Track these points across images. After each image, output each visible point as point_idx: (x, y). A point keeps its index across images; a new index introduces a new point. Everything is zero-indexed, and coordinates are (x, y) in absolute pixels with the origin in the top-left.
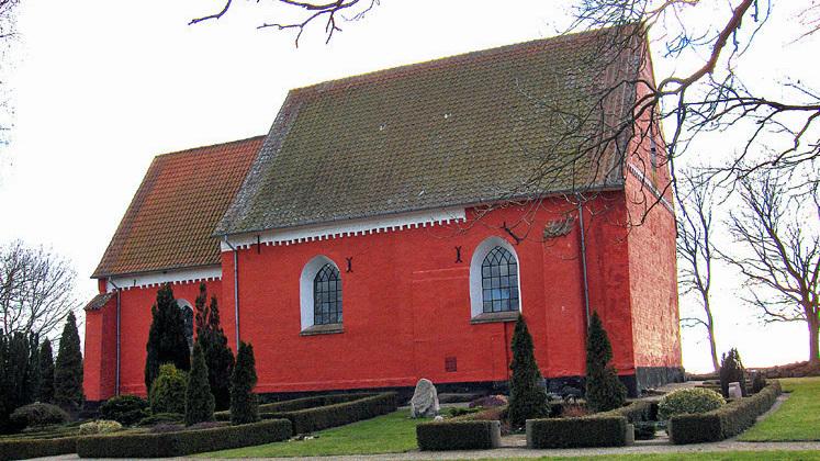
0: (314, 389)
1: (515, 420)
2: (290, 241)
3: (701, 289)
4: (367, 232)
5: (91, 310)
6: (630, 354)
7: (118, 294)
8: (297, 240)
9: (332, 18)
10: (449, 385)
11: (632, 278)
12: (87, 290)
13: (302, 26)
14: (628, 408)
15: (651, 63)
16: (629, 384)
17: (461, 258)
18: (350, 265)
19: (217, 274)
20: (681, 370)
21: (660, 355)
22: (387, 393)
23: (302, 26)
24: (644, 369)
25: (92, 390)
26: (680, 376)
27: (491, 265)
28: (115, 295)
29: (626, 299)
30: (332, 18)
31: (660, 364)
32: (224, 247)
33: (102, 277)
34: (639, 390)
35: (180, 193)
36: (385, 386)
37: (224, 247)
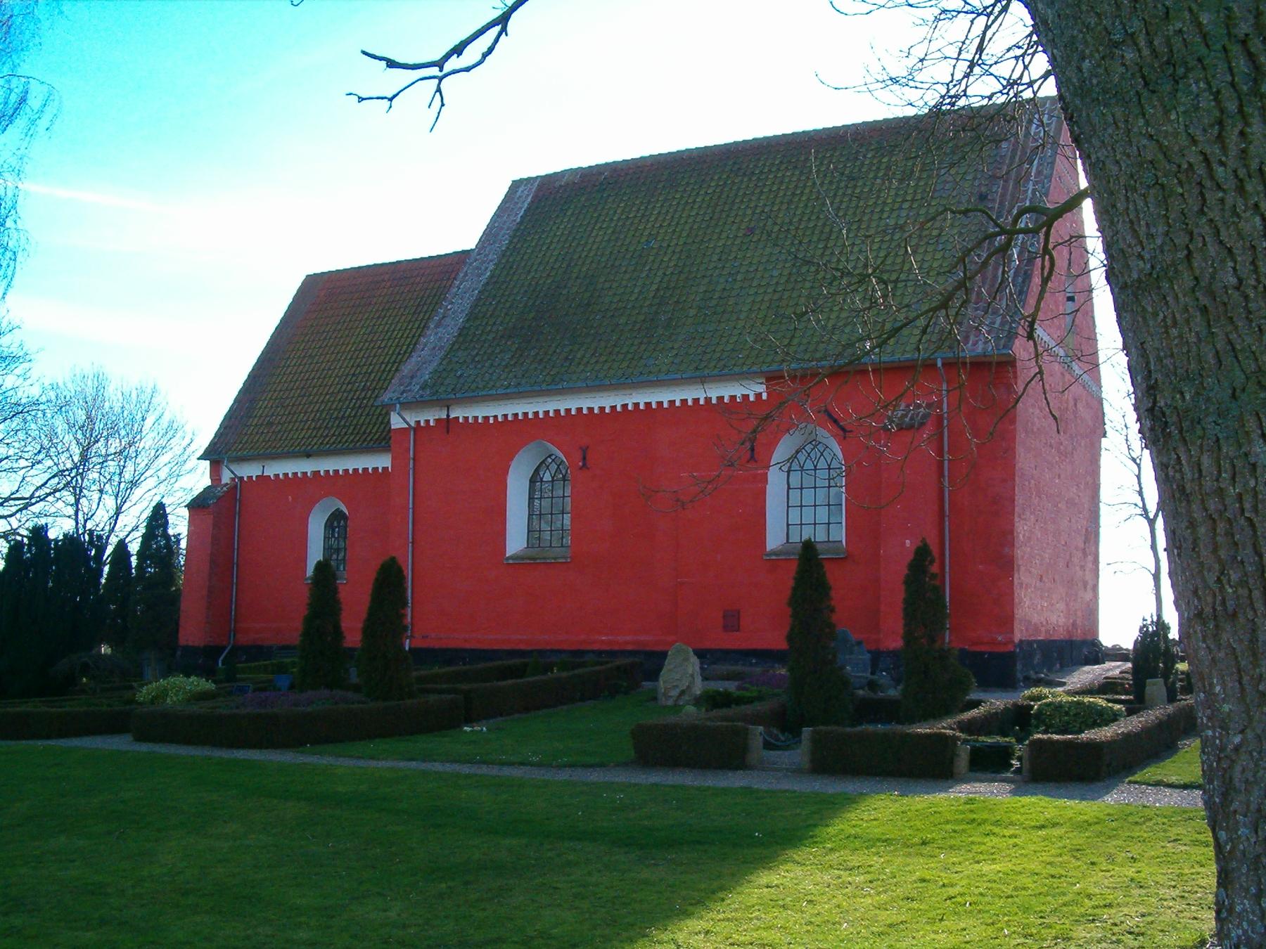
0: (523, 647)
1: (787, 724)
2: (496, 417)
3: (1147, 518)
4: (613, 408)
5: (197, 506)
6: (1007, 621)
7: (240, 485)
8: (516, 415)
9: (439, 90)
10: (531, 702)
11: (1019, 500)
12: (199, 478)
13: (391, 100)
14: (974, 713)
15: (490, 50)
16: (1000, 668)
17: (757, 457)
18: (584, 458)
19: (382, 461)
20: (1095, 644)
21: (1062, 621)
22: (449, 697)
23: (391, 100)
24: (1030, 643)
25: (192, 632)
26: (1095, 653)
27: (815, 469)
28: (233, 489)
29: (1007, 537)
30: (439, 90)
31: (1061, 635)
32: (396, 422)
33: (215, 455)
34: (1020, 676)
35: (344, 345)
36: (629, 648)
37: (396, 422)
